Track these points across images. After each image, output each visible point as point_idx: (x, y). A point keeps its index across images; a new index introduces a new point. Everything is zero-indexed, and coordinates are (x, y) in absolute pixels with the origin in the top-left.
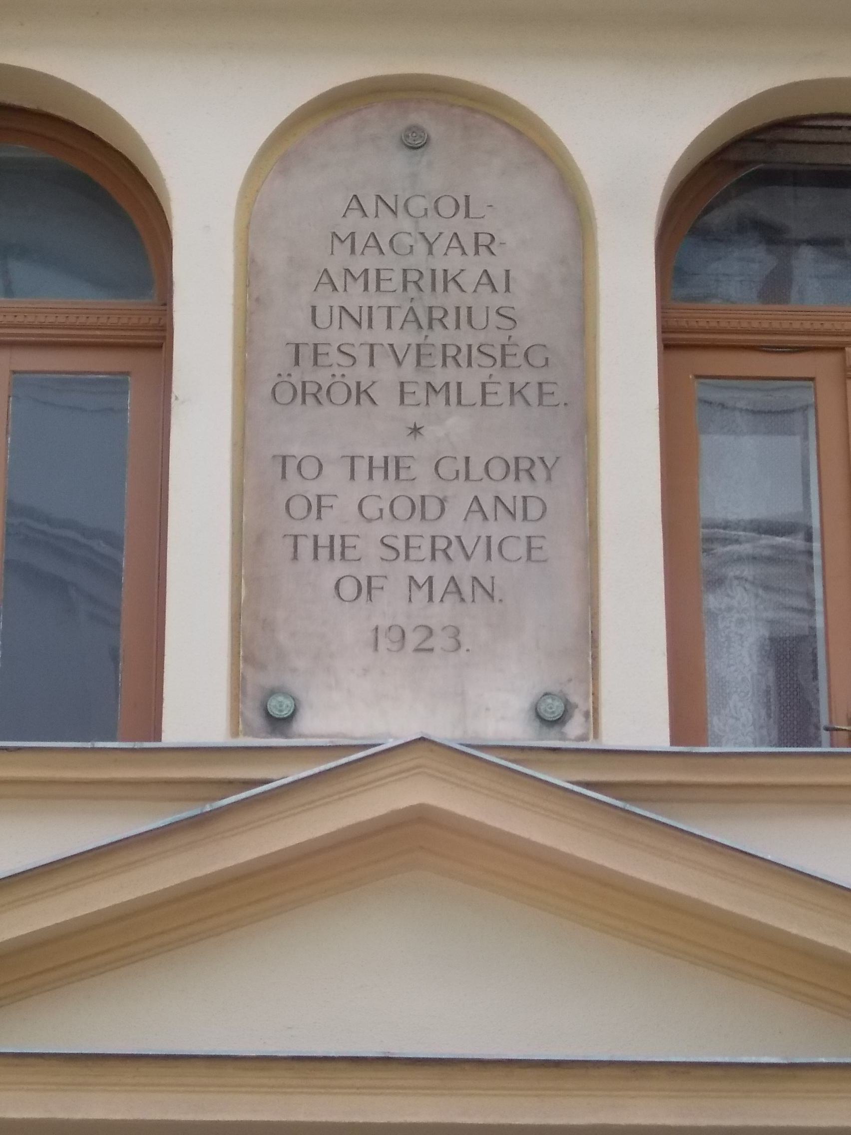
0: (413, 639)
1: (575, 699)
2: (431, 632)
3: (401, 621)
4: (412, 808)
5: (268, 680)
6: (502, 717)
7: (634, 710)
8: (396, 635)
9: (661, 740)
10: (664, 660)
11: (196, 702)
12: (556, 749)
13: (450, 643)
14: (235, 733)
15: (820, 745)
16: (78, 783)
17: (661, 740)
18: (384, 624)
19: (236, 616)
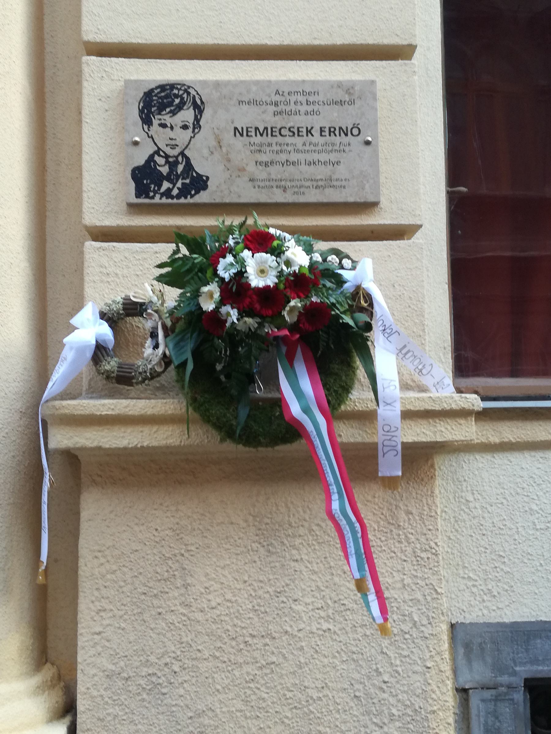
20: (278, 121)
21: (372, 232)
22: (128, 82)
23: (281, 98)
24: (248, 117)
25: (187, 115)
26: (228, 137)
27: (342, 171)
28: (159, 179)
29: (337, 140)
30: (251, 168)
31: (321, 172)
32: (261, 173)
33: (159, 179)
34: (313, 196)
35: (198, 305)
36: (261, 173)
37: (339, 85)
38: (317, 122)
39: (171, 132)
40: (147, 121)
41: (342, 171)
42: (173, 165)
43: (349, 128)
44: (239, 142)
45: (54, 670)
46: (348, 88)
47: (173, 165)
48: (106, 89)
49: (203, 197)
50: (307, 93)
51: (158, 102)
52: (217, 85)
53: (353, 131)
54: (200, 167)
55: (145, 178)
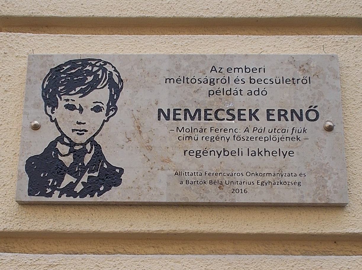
20: (214, 103)
23: (218, 77)
25: (102, 95)
27: (294, 164)
28: (61, 171)
31: (269, 164)
33: (61, 171)
37: (292, 60)
38: (263, 104)
39: (78, 118)
42: (79, 155)
44: (164, 127)
49: (114, 195)
53: (312, 113)
54: (113, 158)
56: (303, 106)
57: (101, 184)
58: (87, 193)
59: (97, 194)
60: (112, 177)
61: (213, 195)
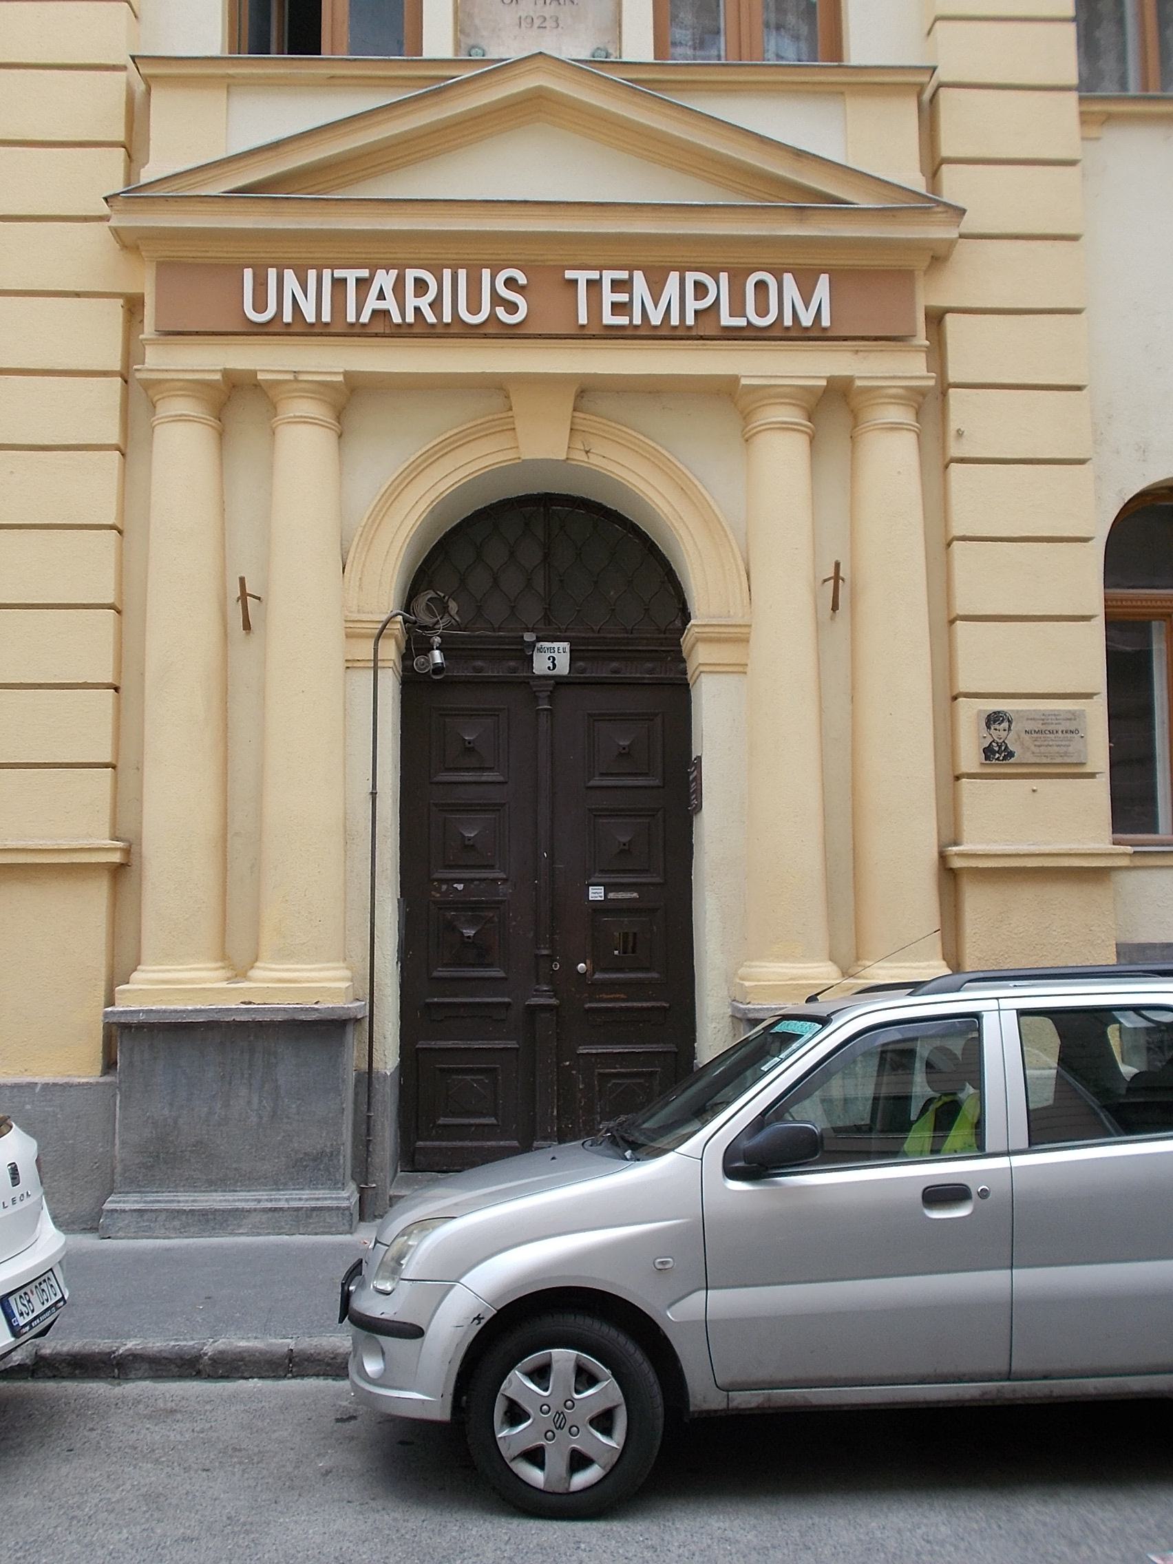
0: (537, 22)
1: (610, 51)
2: (545, 19)
3: (531, 14)
4: (536, 88)
5: (471, 42)
6: (576, 47)
7: (638, 44)
8: (529, 20)
9: (650, 58)
10: (652, 32)
11: (438, 39)
12: (600, 66)
13: (554, 25)
14: (456, 55)
15: (979, 1148)
16: (385, 78)
17: (650, 58)
18: (524, 15)
19: (456, 13)
20: (1043, 728)
21: (478, 1318)
22: (980, 711)
23: (1045, 717)
24: (1030, 726)
25: (1005, 725)
26: (1023, 735)
27: (1071, 749)
28: (994, 752)
29: (1069, 735)
30: (1033, 748)
31: (1063, 749)
32: (1036, 750)
33: (994, 752)
34: (1058, 760)
35: (836, 1072)
36: (1036, 750)
37: (1069, 711)
38: (1060, 728)
39: (999, 732)
40: (989, 728)
41: (1071, 749)
42: (1000, 747)
43: (1073, 729)
44: (1027, 737)
45: (898, 414)
46: (1073, 713)
47: (1000, 747)
48: (970, 713)
49: (1012, 760)
50: (1056, 714)
51: (993, 719)
52: (1017, 711)
53: (1076, 731)
54: (1011, 748)
55: (988, 752)
56: (1073, 729)
57: (627, 1141)
58: (272, 262)
59: (37, 1090)
60: (1011, 754)
61: (1045, 760)
